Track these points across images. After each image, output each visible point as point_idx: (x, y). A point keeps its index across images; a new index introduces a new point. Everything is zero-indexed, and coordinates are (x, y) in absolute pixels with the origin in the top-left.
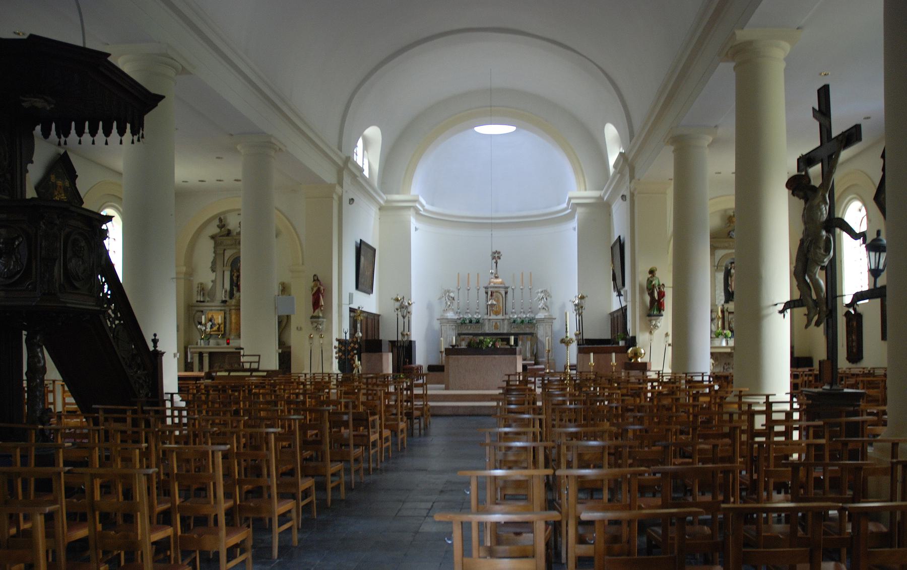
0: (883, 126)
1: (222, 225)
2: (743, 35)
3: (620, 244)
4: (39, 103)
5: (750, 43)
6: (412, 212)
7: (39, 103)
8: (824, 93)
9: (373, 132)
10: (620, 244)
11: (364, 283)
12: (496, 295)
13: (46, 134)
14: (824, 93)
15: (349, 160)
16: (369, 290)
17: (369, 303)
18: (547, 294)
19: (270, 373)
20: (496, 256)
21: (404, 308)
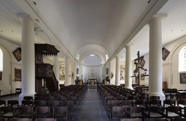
0: (162, 32)
1: (60, 66)
2: (127, 45)
3: (108, 69)
4: (45, 51)
5: (128, 46)
6: (83, 65)
7: (45, 51)
8: (138, 52)
9: (79, 55)
10: (108, 69)
11: (77, 73)
12: (93, 75)
13: (44, 55)
14: (138, 52)
15: (76, 59)
16: (78, 74)
17: (78, 76)
18: (98, 75)
19: (27, 99)
20: (92, 70)
21: (82, 76)
